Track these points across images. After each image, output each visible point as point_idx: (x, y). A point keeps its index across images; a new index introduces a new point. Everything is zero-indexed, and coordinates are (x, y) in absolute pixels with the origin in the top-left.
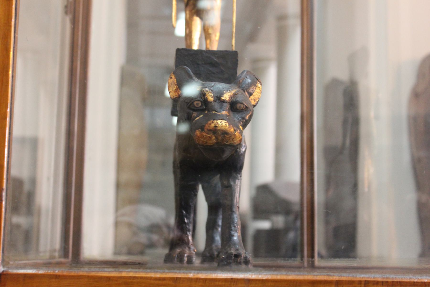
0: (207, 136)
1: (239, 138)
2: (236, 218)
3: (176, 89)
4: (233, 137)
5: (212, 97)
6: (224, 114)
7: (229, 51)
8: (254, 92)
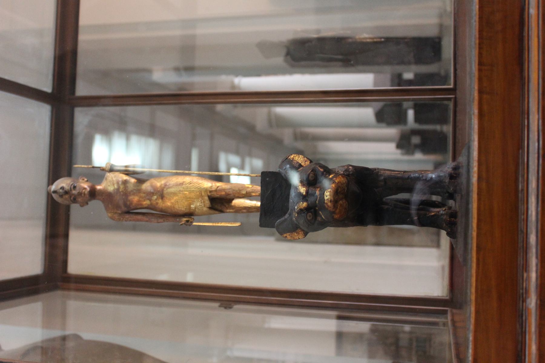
0: (339, 209)
1: (340, 178)
2: (415, 175)
3: (296, 233)
4: (340, 185)
5: (303, 203)
6: (319, 193)
7: (261, 180)
8: (299, 163)
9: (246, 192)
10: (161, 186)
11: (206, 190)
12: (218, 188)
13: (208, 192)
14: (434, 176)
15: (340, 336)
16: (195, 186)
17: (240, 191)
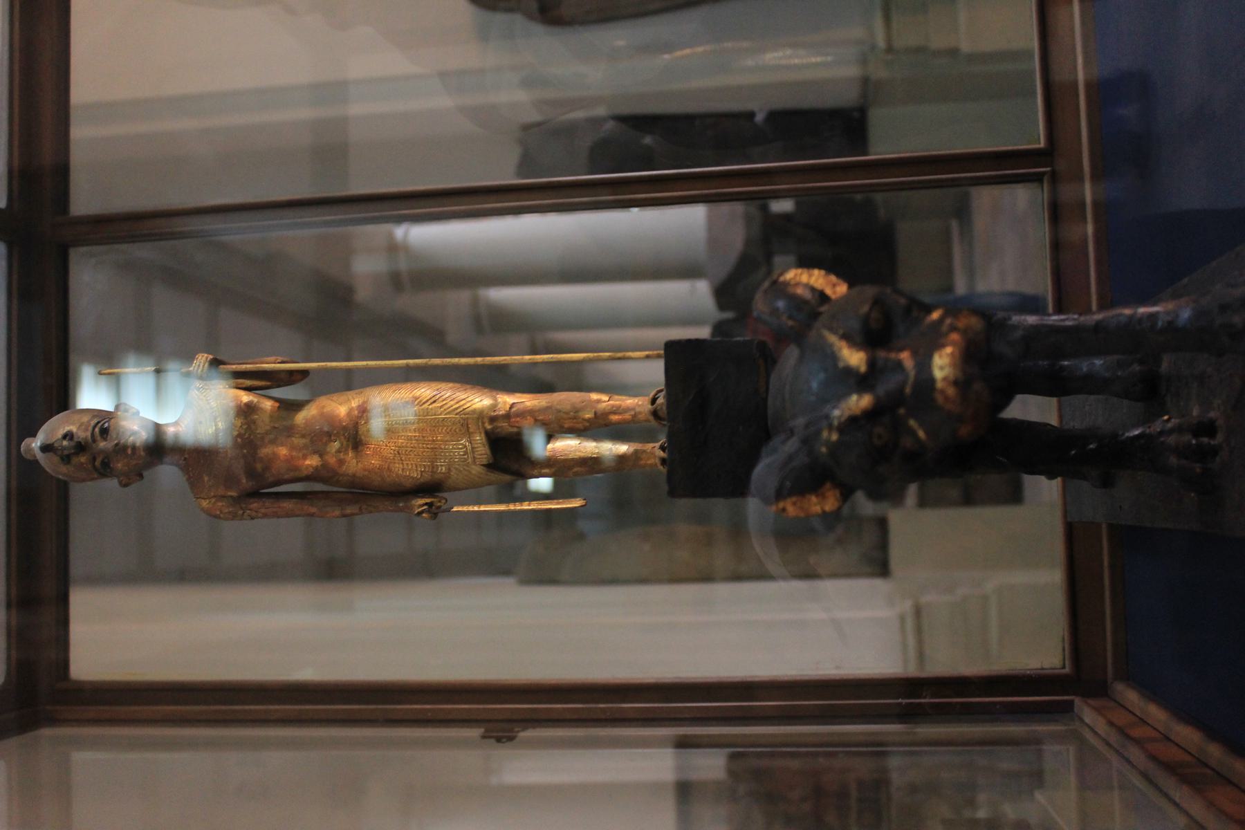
9: (595, 413)
10: (349, 414)
11: (480, 415)
12: (514, 409)
13: (486, 420)
14: (1186, 314)
15: (685, 791)
16: (449, 407)
17: (577, 411)
